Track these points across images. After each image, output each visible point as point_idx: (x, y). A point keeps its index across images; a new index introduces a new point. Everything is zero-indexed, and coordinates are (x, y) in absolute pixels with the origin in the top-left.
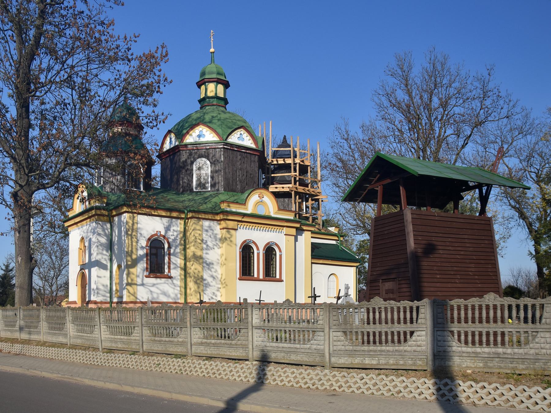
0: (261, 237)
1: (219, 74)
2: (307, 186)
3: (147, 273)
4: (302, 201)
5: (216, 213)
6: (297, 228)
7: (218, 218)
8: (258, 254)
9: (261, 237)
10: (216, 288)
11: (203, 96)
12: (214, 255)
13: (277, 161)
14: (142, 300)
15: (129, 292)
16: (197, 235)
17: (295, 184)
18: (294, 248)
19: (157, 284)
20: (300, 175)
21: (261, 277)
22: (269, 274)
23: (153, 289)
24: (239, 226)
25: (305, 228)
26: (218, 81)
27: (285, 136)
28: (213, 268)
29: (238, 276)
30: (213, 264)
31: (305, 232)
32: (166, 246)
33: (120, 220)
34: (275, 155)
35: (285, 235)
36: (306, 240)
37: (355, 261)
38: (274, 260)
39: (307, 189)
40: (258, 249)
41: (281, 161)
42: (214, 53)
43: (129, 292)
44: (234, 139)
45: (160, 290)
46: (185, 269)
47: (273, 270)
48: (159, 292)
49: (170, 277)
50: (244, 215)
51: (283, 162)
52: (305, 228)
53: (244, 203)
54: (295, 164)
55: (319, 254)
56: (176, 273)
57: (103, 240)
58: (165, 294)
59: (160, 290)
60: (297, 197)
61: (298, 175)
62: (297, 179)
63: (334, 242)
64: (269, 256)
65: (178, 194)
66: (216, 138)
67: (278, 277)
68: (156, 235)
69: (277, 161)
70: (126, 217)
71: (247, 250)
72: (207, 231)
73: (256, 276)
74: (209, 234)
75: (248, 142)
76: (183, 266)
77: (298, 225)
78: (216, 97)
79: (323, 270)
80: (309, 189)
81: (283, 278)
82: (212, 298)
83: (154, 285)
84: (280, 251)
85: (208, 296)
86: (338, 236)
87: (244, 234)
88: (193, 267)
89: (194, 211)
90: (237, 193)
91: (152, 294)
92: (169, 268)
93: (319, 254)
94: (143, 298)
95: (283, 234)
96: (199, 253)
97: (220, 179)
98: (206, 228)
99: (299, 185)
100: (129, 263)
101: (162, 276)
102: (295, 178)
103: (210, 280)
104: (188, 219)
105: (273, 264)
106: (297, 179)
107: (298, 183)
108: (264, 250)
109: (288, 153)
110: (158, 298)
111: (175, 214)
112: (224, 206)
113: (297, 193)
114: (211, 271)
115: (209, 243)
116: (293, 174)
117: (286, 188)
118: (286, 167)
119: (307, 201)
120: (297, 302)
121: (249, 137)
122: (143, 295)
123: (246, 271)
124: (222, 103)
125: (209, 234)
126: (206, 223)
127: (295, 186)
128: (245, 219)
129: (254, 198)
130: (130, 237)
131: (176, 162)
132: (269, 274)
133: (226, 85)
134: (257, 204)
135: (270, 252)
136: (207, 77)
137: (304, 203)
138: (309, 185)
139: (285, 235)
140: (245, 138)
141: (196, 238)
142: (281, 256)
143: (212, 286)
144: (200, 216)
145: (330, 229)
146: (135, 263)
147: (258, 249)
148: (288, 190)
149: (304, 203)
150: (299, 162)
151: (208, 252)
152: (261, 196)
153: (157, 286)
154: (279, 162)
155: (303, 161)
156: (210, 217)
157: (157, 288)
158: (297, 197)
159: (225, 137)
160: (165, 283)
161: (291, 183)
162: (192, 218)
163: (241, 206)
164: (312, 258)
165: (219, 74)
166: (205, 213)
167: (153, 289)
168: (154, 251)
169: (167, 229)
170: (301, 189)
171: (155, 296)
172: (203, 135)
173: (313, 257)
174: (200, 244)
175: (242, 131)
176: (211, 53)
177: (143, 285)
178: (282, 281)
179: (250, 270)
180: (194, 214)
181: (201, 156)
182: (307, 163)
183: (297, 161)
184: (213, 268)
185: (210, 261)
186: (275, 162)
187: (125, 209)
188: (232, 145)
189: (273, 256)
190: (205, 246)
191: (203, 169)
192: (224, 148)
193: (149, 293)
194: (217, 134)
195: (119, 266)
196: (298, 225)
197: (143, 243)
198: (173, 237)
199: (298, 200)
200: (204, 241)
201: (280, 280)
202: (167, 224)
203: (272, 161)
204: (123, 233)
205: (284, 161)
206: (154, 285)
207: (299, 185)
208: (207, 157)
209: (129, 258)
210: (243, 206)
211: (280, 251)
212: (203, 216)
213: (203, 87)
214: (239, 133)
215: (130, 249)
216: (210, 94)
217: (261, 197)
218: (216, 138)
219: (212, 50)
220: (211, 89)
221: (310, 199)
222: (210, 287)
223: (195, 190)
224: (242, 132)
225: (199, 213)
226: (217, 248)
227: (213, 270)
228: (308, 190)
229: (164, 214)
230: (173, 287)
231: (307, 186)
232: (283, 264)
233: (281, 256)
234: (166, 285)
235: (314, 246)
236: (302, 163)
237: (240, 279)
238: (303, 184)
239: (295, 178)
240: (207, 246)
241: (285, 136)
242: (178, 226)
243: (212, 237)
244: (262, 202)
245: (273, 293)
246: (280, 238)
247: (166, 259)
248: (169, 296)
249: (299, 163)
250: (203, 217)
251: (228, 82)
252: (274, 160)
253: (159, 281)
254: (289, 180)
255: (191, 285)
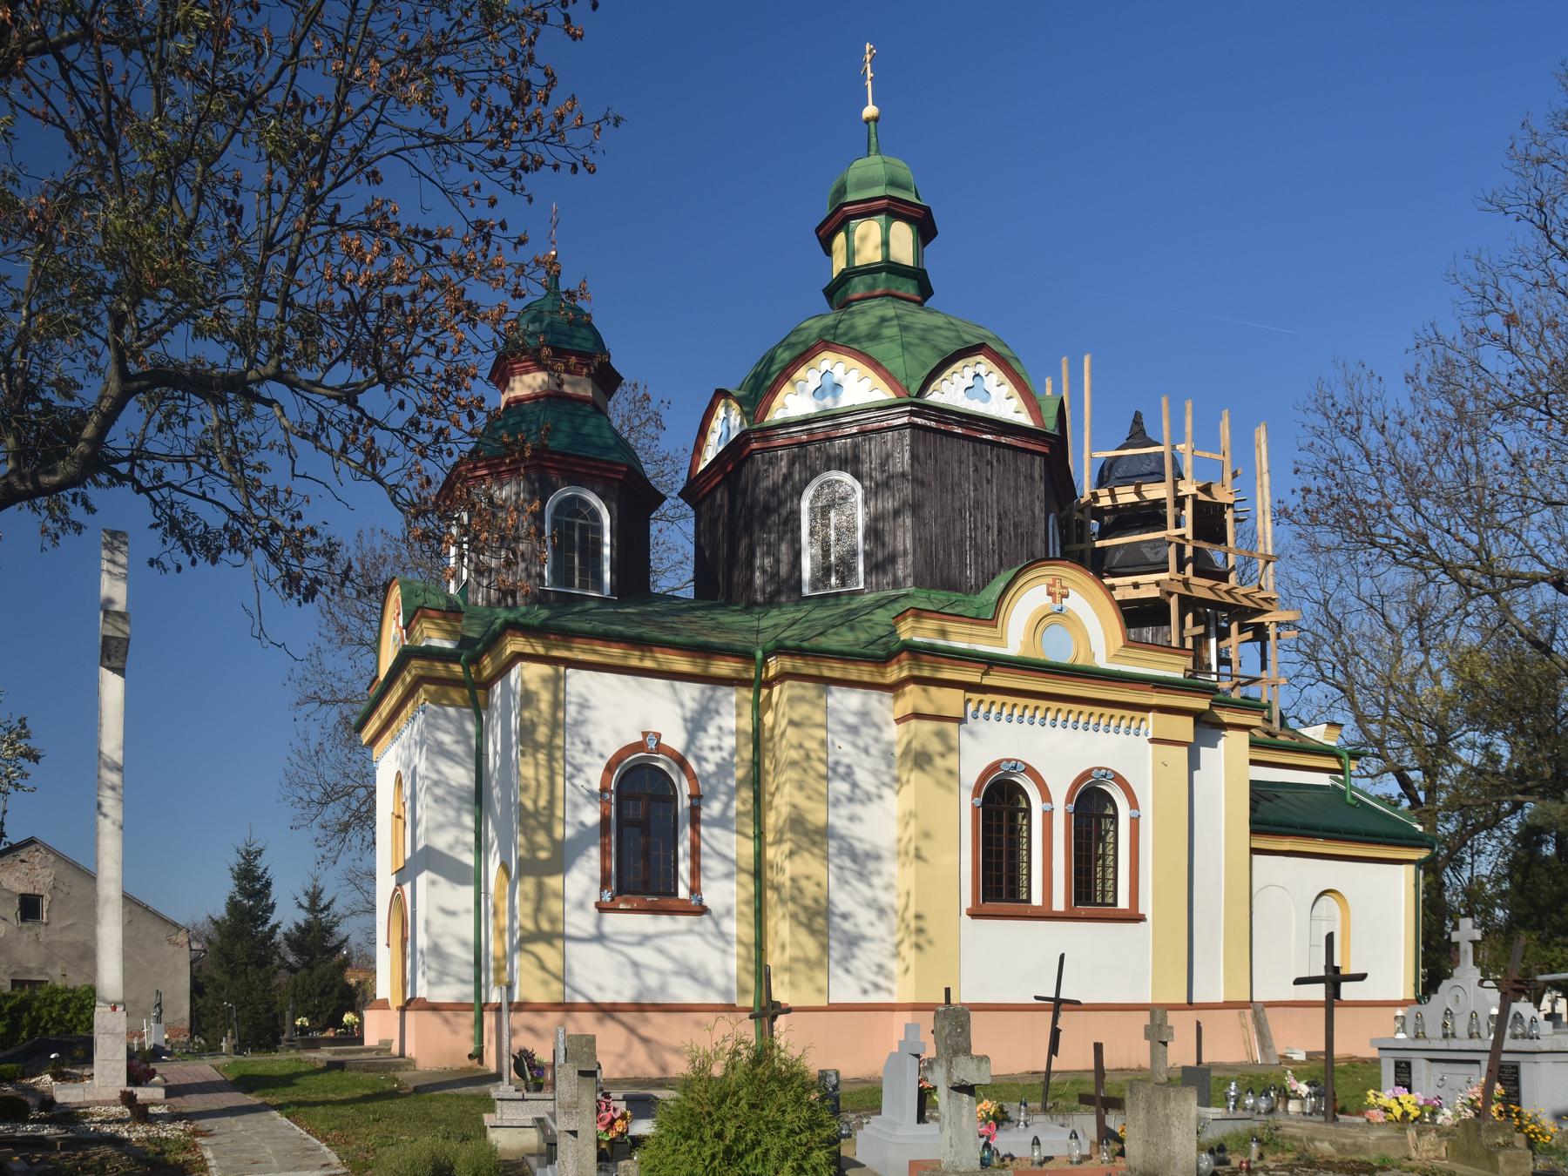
0: (1056, 752)
1: (893, 183)
2: (1223, 577)
3: (607, 897)
4: (1206, 636)
5: (881, 660)
6: (1199, 717)
7: (893, 674)
8: (1048, 816)
9: (1056, 752)
10: (888, 948)
11: (839, 264)
12: (880, 823)
13: (1113, 496)
14: (600, 998)
15: (543, 967)
16: (811, 745)
17: (1181, 568)
18: (1186, 797)
19: (659, 935)
20: (1196, 536)
21: (1059, 904)
22: (1090, 892)
23: (643, 955)
24: (971, 707)
25: (1226, 716)
26: (893, 210)
27: (1138, 416)
28: (879, 873)
29: (967, 902)
30: (878, 858)
31: (1230, 733)
32: (684, 789)
33: (507, 690)
34: (1108, 475)
35: (1153, 741)
36: (1229, 766)
37: (1414, 841)
38: (1110, 838)
39: (1224, 586)
40: (1046, 796)
41: (1126, 496)
42: (876, 119)
43: (543, 967)
44: (951, 392)
45: (672, 959)
46: (758, 873)
47: (1104, 879)
48: (667, 965)
49: (702, 910)
50: (992, 662)
51: (1134, 498)
52: (1226, 716)
53: (990, 618)
54: (1180, 502)
55: (1276, 819)
56: (724, 892)
57: (461, 776)
58: (692, 974)
59: (672, 959)
60: (1189, 618)
61: (1189, 536)
62: (1189, 552)
63: (1323, 779)
64: (1089, 824)
65: (750, 606)
66: (884, 394)
67: (1123, 903)
68: (639, 746)
69: (1113, 496)
70: (529, 674)
71: (1001, 803)
72: (853, 730)
73: (1037, 899)
74: (861, 743)
75: (1002, 402)
76: (749, 863)
77: (1202, 704)
78: (890, 267)
79: (1292, 878)
80: (1236, 589)
81: (1146, 907)
82: (877, 987)
83: (644, 939)
84: (1133, 803)
85: (859, 978)
86: (1338, 757)
87: (994, 738)
88: (786, 865)
89: (798, 652)
90: (967, 593)
91: (637, 975)
92: (696, 872)
93: (1276, 819)
94: (600, 988)
95: (1143, 739)
96: (817, 815)
97: (903, 538)
98: (852, 720)
99: (1195, 574)
100: (543, 855)
101: (670, 902)
102: (1180, 549)
103: (863, 919)
104: (769, 684)
105: (1104, 856)
106: (1189, 552)
107: (1189, 568)
108: (1069, 800)
109: (1153, 466)
110: (663, 989)
111: (723, 667)
112: (908, 631)
113: (1187, 603)
114: (870, 885)
115: (862, 776)
116: (1172, 531)
117: (1147, 587)
118: (1151, 515)
119: (1223, 635)
120: (1323, 973)
121: (1008, 388)
122: (599, 974)
123: (1000, 885)
124: (909, 288)
125: (861, 743)
126: (847, 701)
127: (1180, 577)
128: (994, 680)
129: (1030, 598)
130: (541, 757)
131: (743, 500)
132: (1090, 892)
133: (925, 229)
134: (1042, 621)
135: (1092, 806)
136: (850, 198)
137: (1213, 642)
138: (1232, 576)
139: (1153, 741)
140: (994, 391)
141: (808, 757)
142: (1135, 823)
143: (871, 940)
144: (826, 673)
145: (1308, 732)
146: (562, 859)
147: (1046, 796)
148: (1155, 593)
149: (1213, 642)
150: (1194, 491)
151: (858, 809)
152: (1057, 590)
153: (662, 943)
154: (1121, 500)
155: (1206, 489)
156: (864, 672)
157: (661, 951)
158: (1189, 618)
159: (915, 387)
160: (690, 931)
161: (1167, 570)
162: (782, 677)
163: (977, 629)
164: (1253, 832)
165: (893, 183)
166: (844, 656)
167: (643, 955)
168: (635, 811)
169: (695, 725)
170: (1201, 588)
171: (652, 980)
172: (840, 384)
173: (1259, 826)
174: (826, 778)
175: (983, 364)
176: (867, 121)
177: (600, 938)
178: (1140, 919)
179: (1014, 879)
180: (799, 663)
181: (831, 463)
182: (1222, 495)
183: (1188, 488)
184: (879, 873)
185: (867, 847)
186: (1105, 502)
187: (514, 645)
188: (942, 413)
189: (1107, 824)
190: (841, 787)
191: (836, 516)
192: (913, 426)
193: (628, 970)
194: (889, 377)
195: (505, 866)
196: (1202, 704)
197: (594, 776)
198: (715, 757)
199: (1191, 629)
200: (841, 770)
201: (1134, 917)
202: (691, 705)
203: (1095, 497)
204: (514, 738)
205: (1138, 493)
206: (644, 939)
207: (1195, 574)
208: (850, 462)
209: (541, 838)
210: (985, 631)
211: (1133, 803)
212: (835, 670)
213: (840, 240)
214: (969, 372)
215: (542, 803)
216: (870, 254)
217: (1057, 593)
218: (884, 394)
219: (870, 111)
220: (869, 240)
221: (1234, 627)
222: (866, 945)
223: (806, 591)
224: (982, 370)
225: (818, 663)
226: (881, 788)
227: (876, 880)
228: (1228, 592)
229: (682, 664)
230: (721, 944)
231: (1223, 577)
232: (1144, 857)
233: (1135, 823)
234: (693, 940)
235: (1259, 792)
236: (1202, 497)
237: (974, 915)
238: (1204, 568)
239: (1180, 549)
240: (855, 785)
241: (1138, 416)
242: (731, 716)
243: (873, 751)
244: (1059, 613)
245: (1109, 965)
246: (1130, 752)
247: (685, 835)
248: (706, 983)
249: (1194, 496)
250: (837, 674)
251: (927, 210)
252: (1103, 492)
253: (664, 922)
254: (1160, 558)
255: (780, 927)
